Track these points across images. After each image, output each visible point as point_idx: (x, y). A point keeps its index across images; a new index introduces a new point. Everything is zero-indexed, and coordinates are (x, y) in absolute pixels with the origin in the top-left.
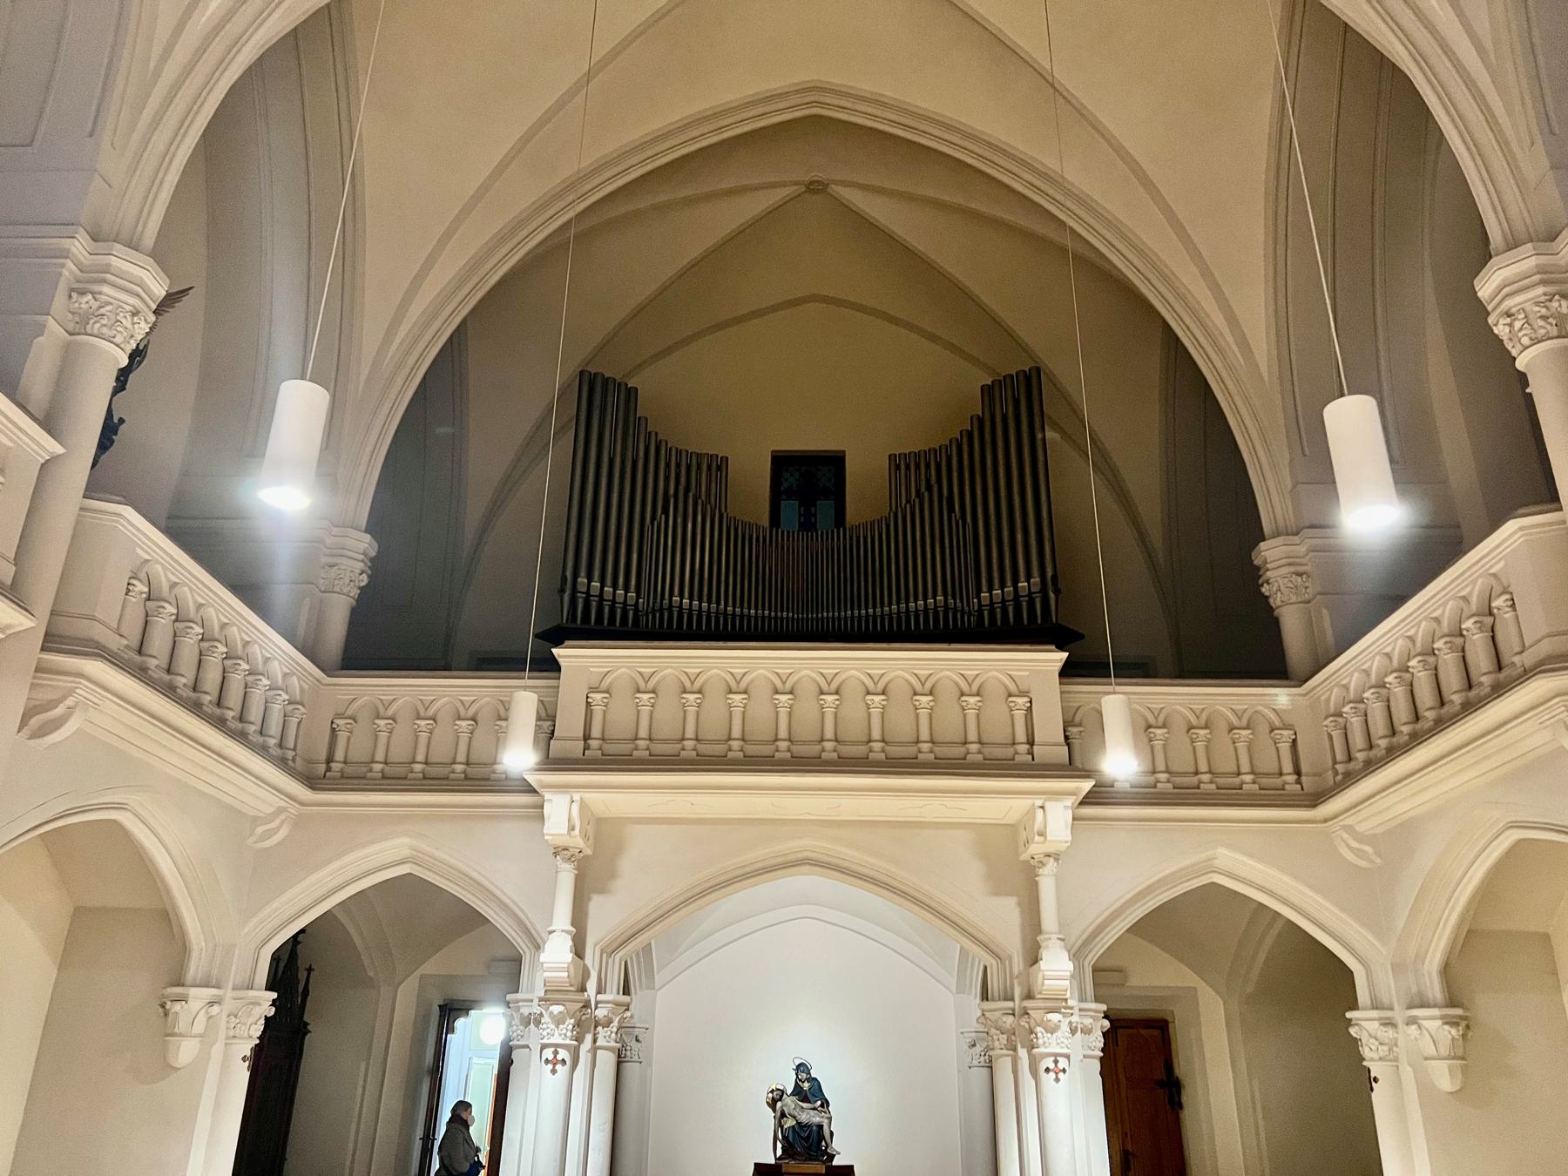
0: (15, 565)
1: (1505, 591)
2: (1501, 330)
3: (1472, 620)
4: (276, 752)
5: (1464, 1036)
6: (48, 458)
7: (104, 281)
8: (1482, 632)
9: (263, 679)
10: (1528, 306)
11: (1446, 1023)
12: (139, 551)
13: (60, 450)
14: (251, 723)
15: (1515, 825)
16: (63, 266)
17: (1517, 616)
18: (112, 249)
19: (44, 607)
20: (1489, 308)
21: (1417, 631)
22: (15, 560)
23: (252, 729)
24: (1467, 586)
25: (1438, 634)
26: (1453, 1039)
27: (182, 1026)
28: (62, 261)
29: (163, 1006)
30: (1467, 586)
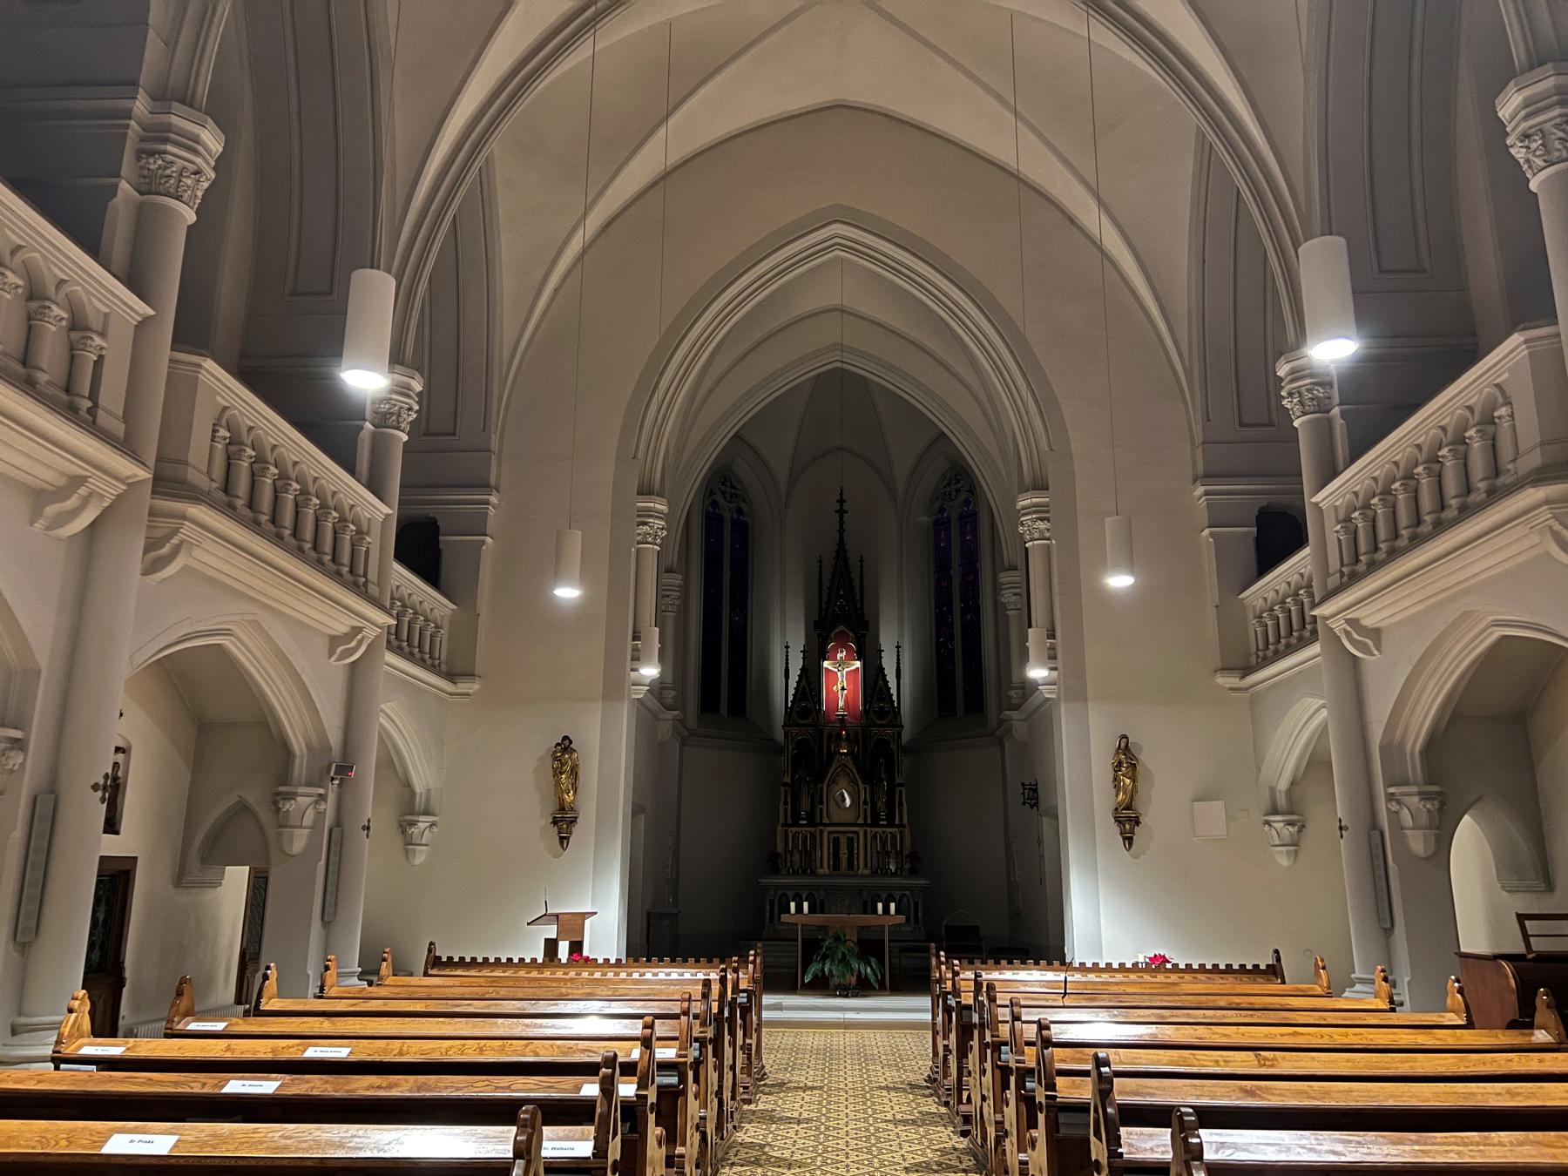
0: (125, 422)
1: (1508, 403)
2: (1518, 153)
3: (1474, 430)
4: (349, 577)
5: (1440, 810)
6: (140, 319)
7: (167, 141)
8: (1457, 459)
9: (247, 449)
10: (1547, 126)
11: (1422, 799)
12: (218, 398)
13: (152, 312)
14: (44, 371)
15: (1497, 624)
16: (128, 126)
17: (1514, 425)
18: (170, 108)
19: (151, 457)
20: (1508, 129)
21: (1451, 420)
22: (123, 418)
23: (264, 518)
24: (1474, 395)
25: (1471, 422)
26: (1429, 811)
27: (294, 821)
28: (127, 122)
29: (275, 803)
30: (1474, 395)
